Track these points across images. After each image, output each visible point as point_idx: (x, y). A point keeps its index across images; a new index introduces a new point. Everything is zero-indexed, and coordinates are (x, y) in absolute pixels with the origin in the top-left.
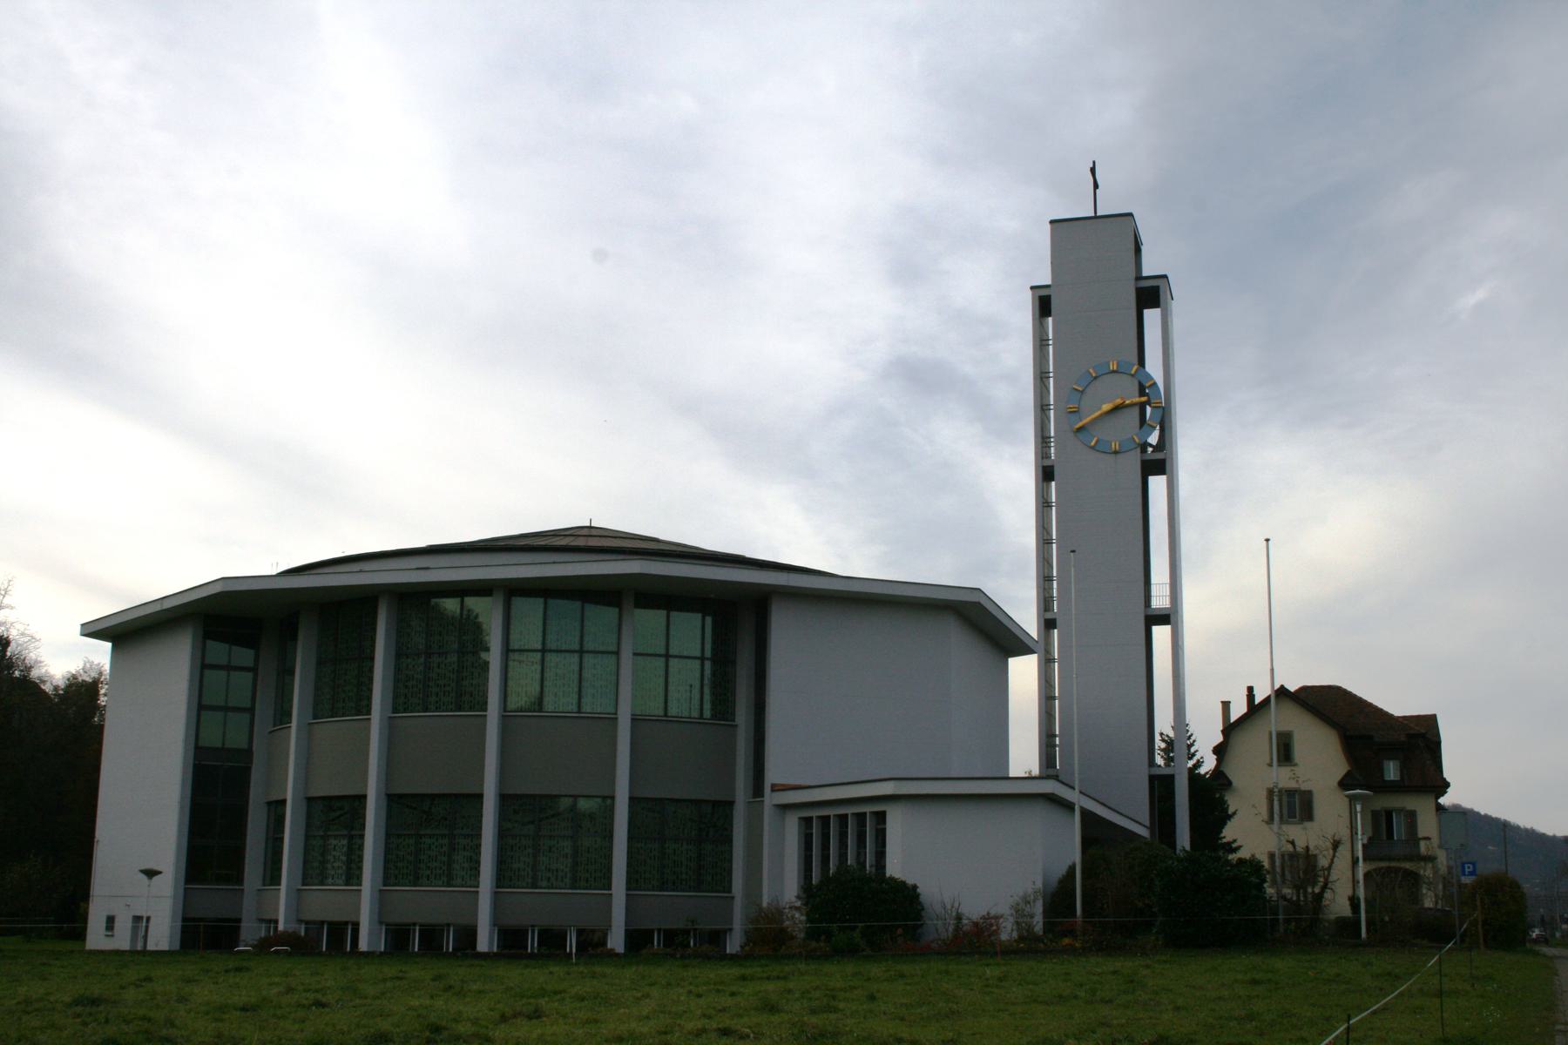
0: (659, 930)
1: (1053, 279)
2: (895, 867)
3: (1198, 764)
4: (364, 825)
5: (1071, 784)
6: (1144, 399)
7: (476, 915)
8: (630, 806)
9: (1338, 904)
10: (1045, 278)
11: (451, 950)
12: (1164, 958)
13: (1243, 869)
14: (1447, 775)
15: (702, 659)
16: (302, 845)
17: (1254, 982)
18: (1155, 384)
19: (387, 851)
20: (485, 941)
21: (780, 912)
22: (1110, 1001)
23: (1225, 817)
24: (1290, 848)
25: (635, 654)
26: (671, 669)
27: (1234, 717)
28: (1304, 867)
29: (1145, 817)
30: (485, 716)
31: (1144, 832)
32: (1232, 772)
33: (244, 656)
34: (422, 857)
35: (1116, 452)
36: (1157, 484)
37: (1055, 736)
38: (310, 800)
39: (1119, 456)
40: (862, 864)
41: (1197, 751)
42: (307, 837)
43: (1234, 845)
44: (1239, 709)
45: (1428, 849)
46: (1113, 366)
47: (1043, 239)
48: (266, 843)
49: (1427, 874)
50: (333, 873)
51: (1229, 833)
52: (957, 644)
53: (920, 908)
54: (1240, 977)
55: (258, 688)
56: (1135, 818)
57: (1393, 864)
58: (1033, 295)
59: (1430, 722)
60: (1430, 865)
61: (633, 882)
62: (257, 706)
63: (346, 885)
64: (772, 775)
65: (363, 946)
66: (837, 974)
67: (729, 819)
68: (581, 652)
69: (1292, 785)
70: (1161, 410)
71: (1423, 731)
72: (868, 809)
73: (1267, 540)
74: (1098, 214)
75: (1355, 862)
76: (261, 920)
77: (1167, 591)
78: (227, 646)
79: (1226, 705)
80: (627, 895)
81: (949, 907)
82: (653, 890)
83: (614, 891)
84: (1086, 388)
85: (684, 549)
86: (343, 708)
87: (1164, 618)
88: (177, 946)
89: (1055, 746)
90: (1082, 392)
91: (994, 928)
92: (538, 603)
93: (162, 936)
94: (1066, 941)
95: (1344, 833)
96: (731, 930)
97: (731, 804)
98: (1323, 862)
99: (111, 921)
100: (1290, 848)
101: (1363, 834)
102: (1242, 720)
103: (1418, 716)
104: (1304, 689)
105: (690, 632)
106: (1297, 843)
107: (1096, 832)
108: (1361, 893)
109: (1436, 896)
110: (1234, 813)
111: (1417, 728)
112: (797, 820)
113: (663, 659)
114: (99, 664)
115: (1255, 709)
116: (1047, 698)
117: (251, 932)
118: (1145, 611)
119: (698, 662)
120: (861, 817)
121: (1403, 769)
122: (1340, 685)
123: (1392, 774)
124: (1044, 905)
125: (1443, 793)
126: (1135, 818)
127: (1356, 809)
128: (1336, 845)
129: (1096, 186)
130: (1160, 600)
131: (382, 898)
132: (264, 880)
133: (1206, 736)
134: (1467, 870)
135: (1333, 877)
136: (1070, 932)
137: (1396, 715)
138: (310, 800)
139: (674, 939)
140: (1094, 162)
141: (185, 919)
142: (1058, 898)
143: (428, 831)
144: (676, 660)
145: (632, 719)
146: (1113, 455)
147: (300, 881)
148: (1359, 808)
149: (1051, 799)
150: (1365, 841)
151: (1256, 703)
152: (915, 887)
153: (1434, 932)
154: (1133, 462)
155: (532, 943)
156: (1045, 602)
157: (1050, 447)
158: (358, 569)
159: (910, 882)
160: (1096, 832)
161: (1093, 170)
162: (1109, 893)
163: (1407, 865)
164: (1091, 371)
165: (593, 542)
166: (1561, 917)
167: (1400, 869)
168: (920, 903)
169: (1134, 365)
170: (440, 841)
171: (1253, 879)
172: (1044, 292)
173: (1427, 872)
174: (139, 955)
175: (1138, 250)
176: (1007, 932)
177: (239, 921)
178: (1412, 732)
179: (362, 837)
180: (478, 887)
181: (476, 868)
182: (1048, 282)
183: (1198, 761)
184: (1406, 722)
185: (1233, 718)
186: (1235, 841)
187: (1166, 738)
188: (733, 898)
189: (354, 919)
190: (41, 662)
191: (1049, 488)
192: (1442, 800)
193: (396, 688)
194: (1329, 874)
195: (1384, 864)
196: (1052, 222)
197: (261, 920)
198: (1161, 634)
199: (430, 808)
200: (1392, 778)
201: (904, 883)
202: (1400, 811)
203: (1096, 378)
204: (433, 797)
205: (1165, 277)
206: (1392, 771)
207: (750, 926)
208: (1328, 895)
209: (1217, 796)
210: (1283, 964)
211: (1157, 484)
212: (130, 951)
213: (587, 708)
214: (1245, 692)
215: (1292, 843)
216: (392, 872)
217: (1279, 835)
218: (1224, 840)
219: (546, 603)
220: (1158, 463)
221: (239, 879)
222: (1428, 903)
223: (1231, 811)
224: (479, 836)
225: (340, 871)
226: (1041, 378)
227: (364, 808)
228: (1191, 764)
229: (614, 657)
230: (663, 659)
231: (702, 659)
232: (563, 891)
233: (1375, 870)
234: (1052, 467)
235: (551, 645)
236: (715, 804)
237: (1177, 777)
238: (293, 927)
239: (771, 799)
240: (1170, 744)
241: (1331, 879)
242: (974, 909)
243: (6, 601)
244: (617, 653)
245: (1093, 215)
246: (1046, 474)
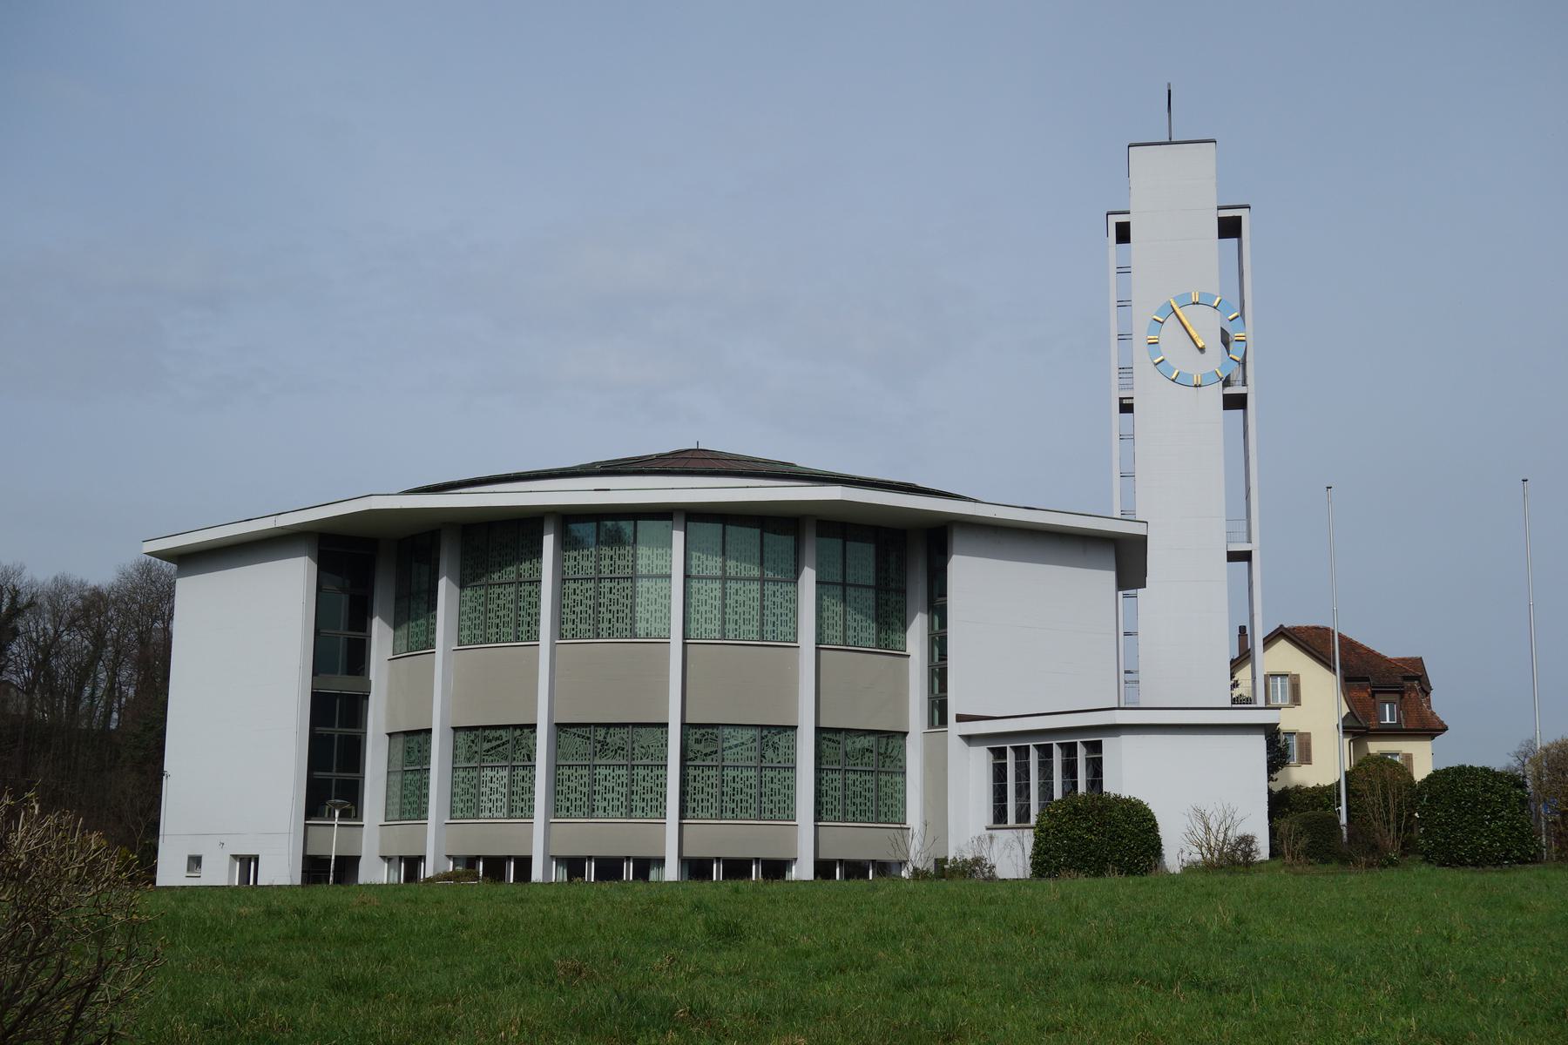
88: (298, 881)
90: (1162, 323)
92: (716, 528)
99: (195, 862)
143: (604, 761)
170: (617, 772)
178: (1406, 674)
189: (522, 853)
199: (605, 738)
212: (542, 884)
216: (557, 807)
219: (724, 529)
232: (408, 822)
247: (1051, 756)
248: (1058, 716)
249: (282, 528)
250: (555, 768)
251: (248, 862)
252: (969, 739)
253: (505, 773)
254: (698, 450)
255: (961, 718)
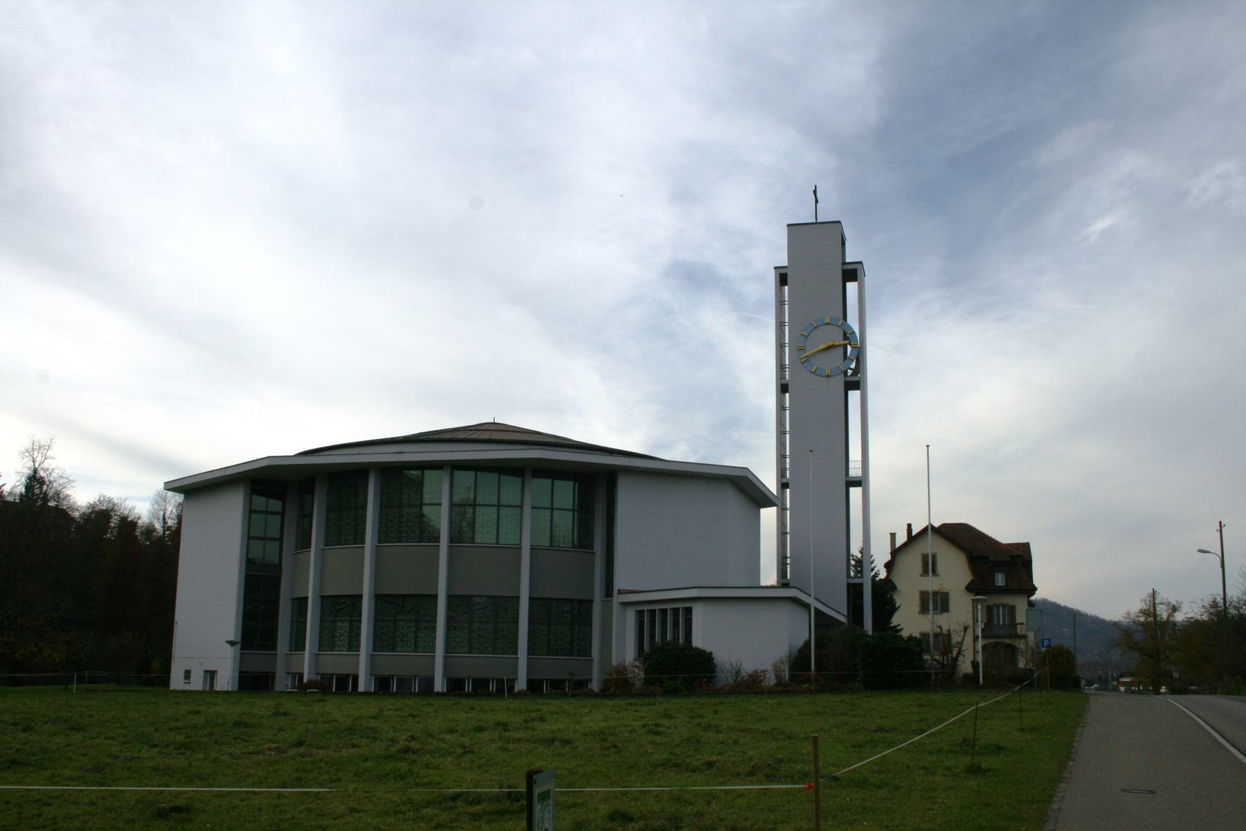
0: (493, 679)
1: (788, 263)
2: (698, 641)
3: (876, 575)
4: (360, 615)
5: (808, 593)
6: (847, 342)
7: (434, 671)
8: (530, 603)
9: (965, 667)
10: (784, 261)
11: (417, 691)
12: (865, 695)
13: (911, 643)
14: (1035, 582)
15: (573, 510)
16: (289, 627)
17: (921, 706)
18: (854, 332)
19: (375, 629)
20: (439, 685)
21: (625, 668)
22: (845, 714)
23: (893, 609)
24: (939, 630)
25: (533, 508)
26: (554, 517)
27: (898, 544)
28: (944, 641)
29: (844, 610)
30: (439, 546)
31: (843, 619)
32: (896, 580)
33: (275, 505)
34: (397, 634)
35: (828, 376)
36: (854, 396)
37: (787, 558)
38: (323, 598)
39: (830, 378)
40: (676, 638)
41: (875, 567)
42: (322, 621)
43: (898, 628)
44: (901, 539)
45: (1021, 630)
46: (827, 321)
47: (781, 239)
48: (292, 625)
49: (1021, 646)
50: (339, 643)
51: (896, 620)
52: (732, 502)
53: (713, 666)
54: (913, 703)
55: (286, 525)
56: (839, 611)
57: (1000, 640)
58: (776, 273)
59: (1026, 547)
60: (1022, 641)
61: (531, 651)
62: (285, 537)
63: (349, 651)
64: (619, 584)
65: (361, 688)
66: (662, 704)
67: (590, 611)
68: (499, 506)
69: (937, 588)
70: (857, 350)
71: (1020, 554)
72: (680, 605)
73: (928, 446)
74: (818, 221)
75: (976, 638)
76: (288, 673)
77: (859, 465)
78: (265, 499)
79: (893, 536)
80: (528, 658)
81: (734, 665)
82: (543, 655)
83: (519, 655)
84: (810, 333)
85: (569, 442)
86: (345, 539)
87: (857, 483)
88: (236, 689)
89: (786, 564)
90: (807, 337)
91: (762, 678)
92: (471, 474)
93: (226, 680)
94: (805, 686)
95: (970, 622)
96: (591, 680)
97: (591, 601)
98: (956, 639)
99: (188, 674)
100: (939, 630)
101: (982, 622)
102: (904, 546)
103: (1018, 544)
104: (944, 525)
105: (565, 492)
106: (943, 627)
107: (823, 621)
108: (980, 658)
109: (1026, 660)
110: (899, 607)
111: (1016, 551)
112: (634, 612)
113: (549, 511)
114: (109, 498)
115: (912, 539)
116: (782, 533)
117: (282, 682)
118: (846, 478)
119: (571, 513)
120: (676, 611)
121: (1008, 578)
122: (967, 522)
123: (1000, 581)
124: (789, 666)
125: (1033, 594)
126: (839, 611)
127: (977, 607)
128: (966, 629)
129: (817, 201)
130: (855, 471)
131: (372, 658)
132: (290, 648)
133: (880, 555)
134: (1045, 644)
135: (963, 648)
136: (808, 680)
137: (1003, 542)
138: (323, 598)
139: (556, 684)
140: (816, 187)
141: (241, 672)
142: (799, 660)
144: (557, 511)
145: (531, 549)
146: (826, 378)
147: (317, 649)
148: (979, 607)
149: (794, 600)
150: (983, 627)
151: (913, 535)
152: (711, 654)
153: (1021, 680)
154: (839, 382)
155: (468, 687)
156: (781, 472)
157: (785, 371)
158: (357, 452)
159: (708, 650)
160: (823, 621)
161: (815, 192)
162: (831, 657)
163: (1008, 641)
164: (813, 323)
165: (495, 436)
166: (1112, 676)
167: (1002, 643)
168: (714, 663)
169: (840, 320)
170: (409, 624)
171: (917, 649)
172: (783, 271)
173: (1020, 645)
174: (210, 692)
175: (843, 244)
176: (771, 680)
177: (275, 673)
179: (360, 621)
180: (434, 653)
181: (433, 642)
182: (786, 264)
183: (876, 573)
184: (1010, 548)
185: (898, 545)
186: (899, 625)
187: (856, 558)
188: (592, 660)
189: (355, 673)
190: (70, 496)
191: (784, 397)
192: (1033, 598)
193: (380, 527)
194: (962, 645)
195: (993, 640)
196: (788, 225)
197: (288, 673)
198: (855, 493)
200: (1000, 584)
201: (704, 651)
202: (1004, 606)
203: (816, 328)
204: (405, 596)
205: (861, 263)
206: (1000, 580)
207: (607, 677)
208: (961, 658)
209: (889, 596)
210: (937, 697)
211: (854, 396)
212: (202, 692)
213: (502, 541)
214: (906, 527)
215: (940, 627)
216: (380, 642)
217: (932, 622)
218: (892, 625)
220: (855, 382)
221: (274, 648)
222: (1021, 665)
223: (897, 605)
224: (435, 621)
225: (344, 642)
226: (780, 326)
227: (361, 603)
228: (873, 574)
229: (519, 509)
230: (549, 511)
231: (573, 510)
232: (401, 654)
233: (988, 644)
234: (787, 384)
235: (503, 511)
236: (581, 602)
237: (865, 585)
238: (314, 677)
239: (617, 599)
240: (859, 563)
241: (963, 649)
242: (748, 667)
243: (49, 454)
244: (521, 507)
245: (815, 221)
246: (783, 388)
247: (666, 615)
248: (669, 588)
249: (229, 475)
250: (449, 620)
251: (211, 675)
252: (626, 604)
253: (347, 624)
254: (494, 423)
255: (620, 592)
